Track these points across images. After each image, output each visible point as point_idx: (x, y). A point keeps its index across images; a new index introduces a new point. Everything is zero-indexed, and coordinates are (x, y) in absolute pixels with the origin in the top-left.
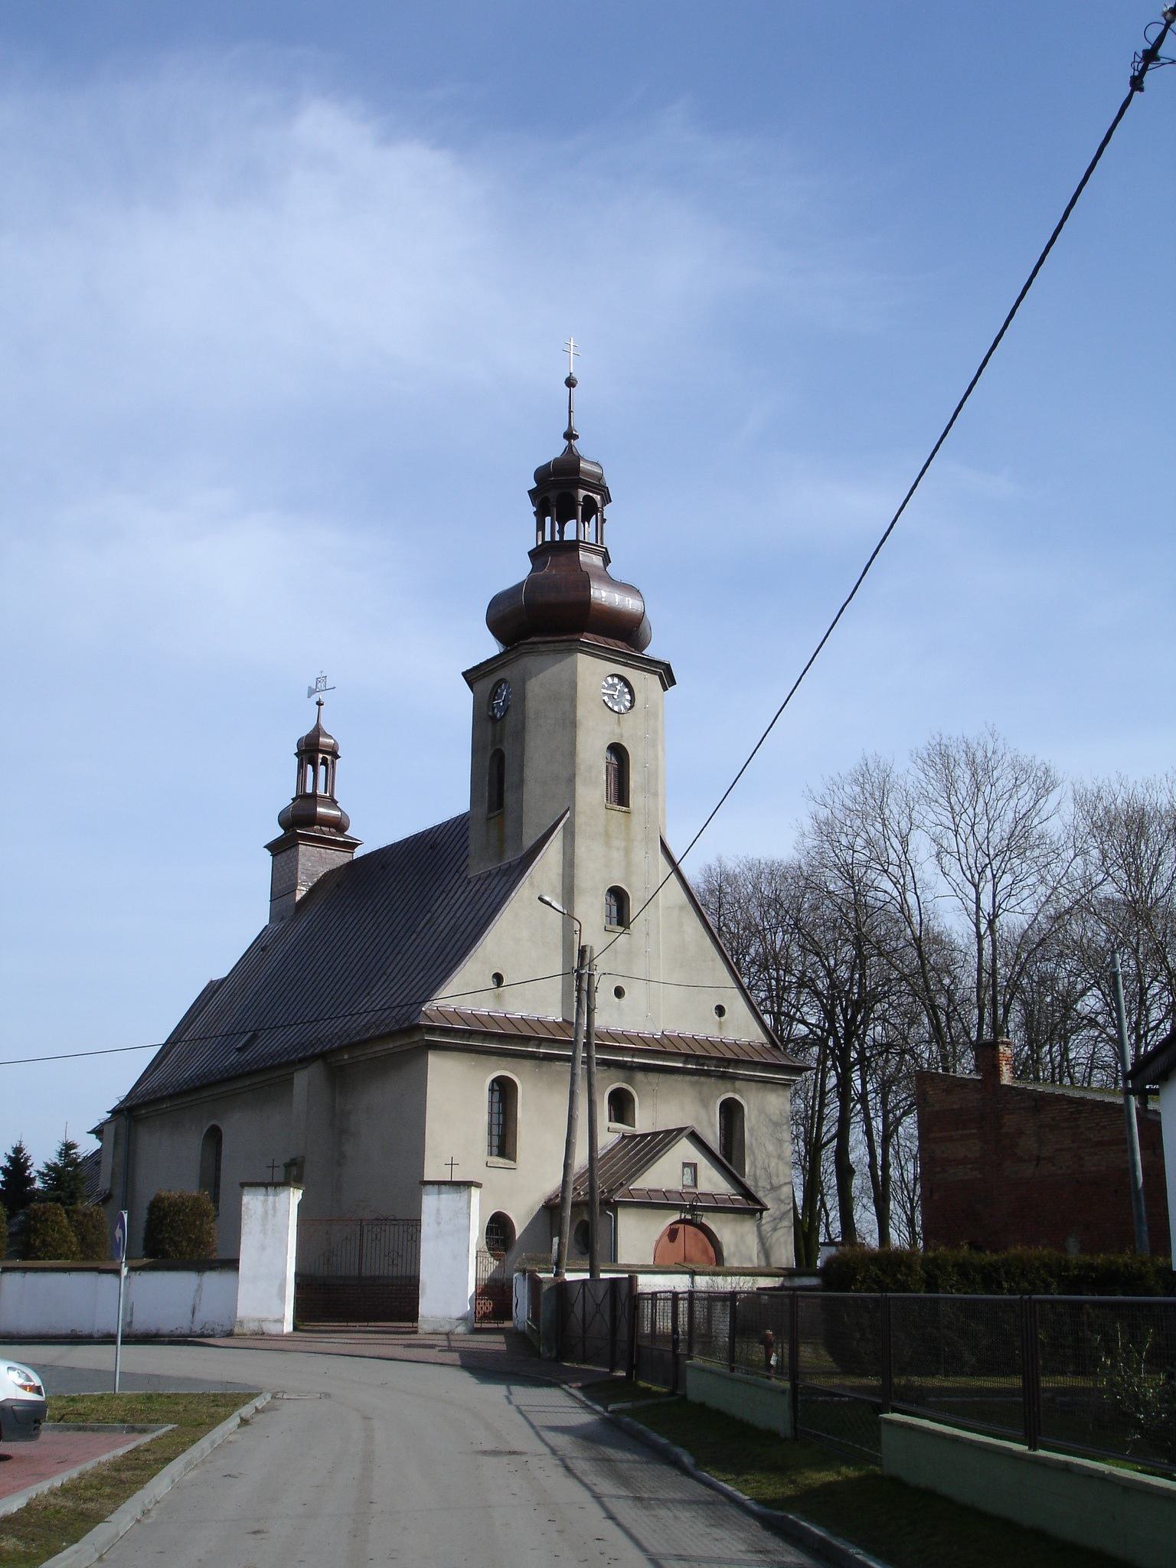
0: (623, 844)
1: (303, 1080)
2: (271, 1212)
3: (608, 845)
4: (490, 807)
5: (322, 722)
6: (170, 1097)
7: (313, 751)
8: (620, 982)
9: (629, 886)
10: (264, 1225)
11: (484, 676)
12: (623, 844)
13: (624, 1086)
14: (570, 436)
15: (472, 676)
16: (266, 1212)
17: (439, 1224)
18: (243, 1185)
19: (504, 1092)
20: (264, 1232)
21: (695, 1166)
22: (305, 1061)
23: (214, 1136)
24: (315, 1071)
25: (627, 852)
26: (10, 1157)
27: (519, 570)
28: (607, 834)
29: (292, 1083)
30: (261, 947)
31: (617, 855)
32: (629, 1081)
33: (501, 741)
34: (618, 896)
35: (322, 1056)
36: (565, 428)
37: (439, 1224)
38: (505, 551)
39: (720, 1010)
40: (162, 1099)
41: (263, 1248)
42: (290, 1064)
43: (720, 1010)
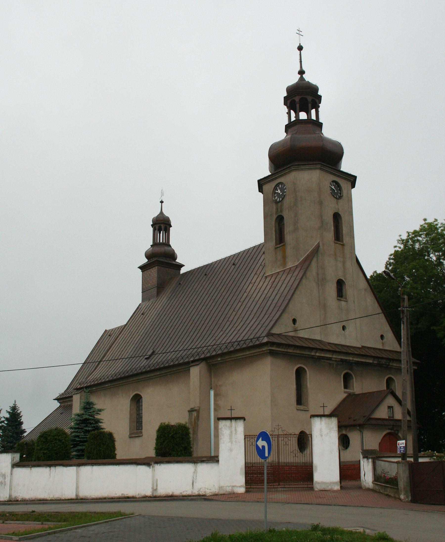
0: (342, 260)
1: (195, 372)
2: (234, 432)
3: (336, 259)
4: (276, 242)
5: (163, 211)
6: (110, 381)
7: (162, 224)
8: (344, 324)
9: (345, 279)
10: (230, 439)
11: (269, 181)
12: (342, 260)
13: (349, 371)
14: (301, 72)
15: (262, 184)
16: (231, 432)
17: (322, 436)
18: (313, 416)
19: (300, 374)
20: (231, 442)
21: (392, 407)
22: (196, 362)
23: (137, 400)
24: (203, 365)
25: (344, 263)
26: (9, 412)
27: (280, 135)
28: (335, 255)
29: (189, 372)
30: (139, 313)
31: (340, 265)
32: (351, 369)
33: (281, 211)
34: (340, 284)
35: (205, 359)
36: (298, 69)
37: (322, 436)
38: (274, 125)
39: (382, 337)
40: (105, 383)
41: (231, 450)
42: (188, 363)
43: (382, 337)
